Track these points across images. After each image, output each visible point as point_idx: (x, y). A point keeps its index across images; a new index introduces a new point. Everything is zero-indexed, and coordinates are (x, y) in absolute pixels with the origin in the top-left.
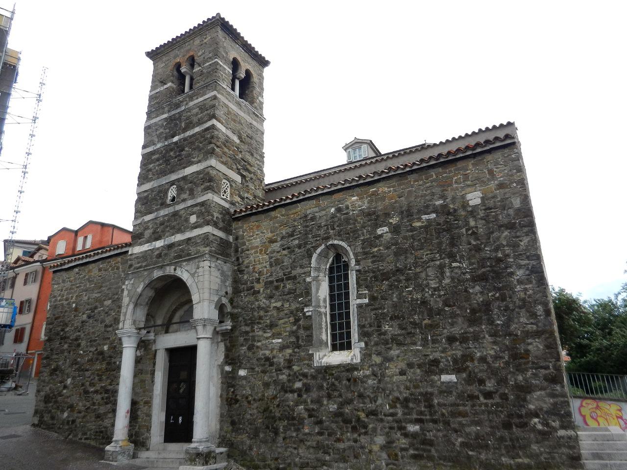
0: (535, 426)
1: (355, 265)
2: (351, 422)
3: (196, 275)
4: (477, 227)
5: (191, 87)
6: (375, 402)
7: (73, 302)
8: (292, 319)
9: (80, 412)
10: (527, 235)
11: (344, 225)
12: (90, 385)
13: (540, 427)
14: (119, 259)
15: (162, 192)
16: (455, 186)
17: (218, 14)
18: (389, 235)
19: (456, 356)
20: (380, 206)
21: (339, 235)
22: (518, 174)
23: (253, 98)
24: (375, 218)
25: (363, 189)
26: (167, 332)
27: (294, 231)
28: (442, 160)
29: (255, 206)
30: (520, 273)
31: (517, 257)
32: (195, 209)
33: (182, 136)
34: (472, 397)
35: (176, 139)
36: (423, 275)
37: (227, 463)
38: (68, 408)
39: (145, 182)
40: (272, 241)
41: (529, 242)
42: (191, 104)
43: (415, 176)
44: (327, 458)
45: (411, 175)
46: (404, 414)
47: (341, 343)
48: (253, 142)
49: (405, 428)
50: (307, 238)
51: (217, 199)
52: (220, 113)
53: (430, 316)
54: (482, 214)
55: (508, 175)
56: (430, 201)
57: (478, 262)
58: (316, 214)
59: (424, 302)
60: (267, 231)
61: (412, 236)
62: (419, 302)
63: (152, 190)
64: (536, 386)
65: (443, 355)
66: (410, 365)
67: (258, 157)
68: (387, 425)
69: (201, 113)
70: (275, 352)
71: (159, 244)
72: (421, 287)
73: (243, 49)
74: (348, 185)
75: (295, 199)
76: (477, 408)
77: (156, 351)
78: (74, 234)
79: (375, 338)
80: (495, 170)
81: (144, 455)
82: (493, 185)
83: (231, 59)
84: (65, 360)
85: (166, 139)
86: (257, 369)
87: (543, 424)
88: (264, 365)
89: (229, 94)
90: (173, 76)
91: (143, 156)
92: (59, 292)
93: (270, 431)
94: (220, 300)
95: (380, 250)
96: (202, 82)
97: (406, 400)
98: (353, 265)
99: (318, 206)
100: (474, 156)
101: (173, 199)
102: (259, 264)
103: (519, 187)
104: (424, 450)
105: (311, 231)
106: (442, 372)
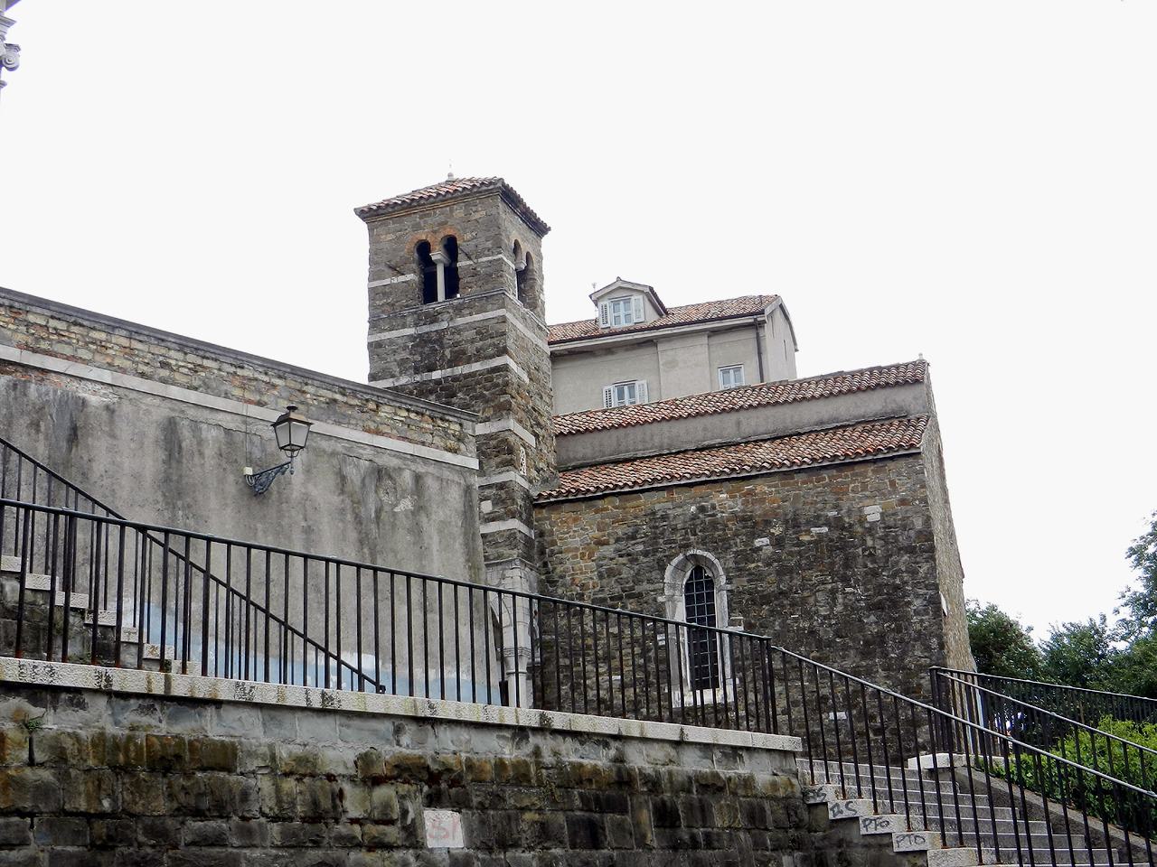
35: (436, 375)
40: (600, 543)
42: (460, 321)
50: (657, 543)
56: (822, 510)
82: (894, 499)
85: (417, 371)
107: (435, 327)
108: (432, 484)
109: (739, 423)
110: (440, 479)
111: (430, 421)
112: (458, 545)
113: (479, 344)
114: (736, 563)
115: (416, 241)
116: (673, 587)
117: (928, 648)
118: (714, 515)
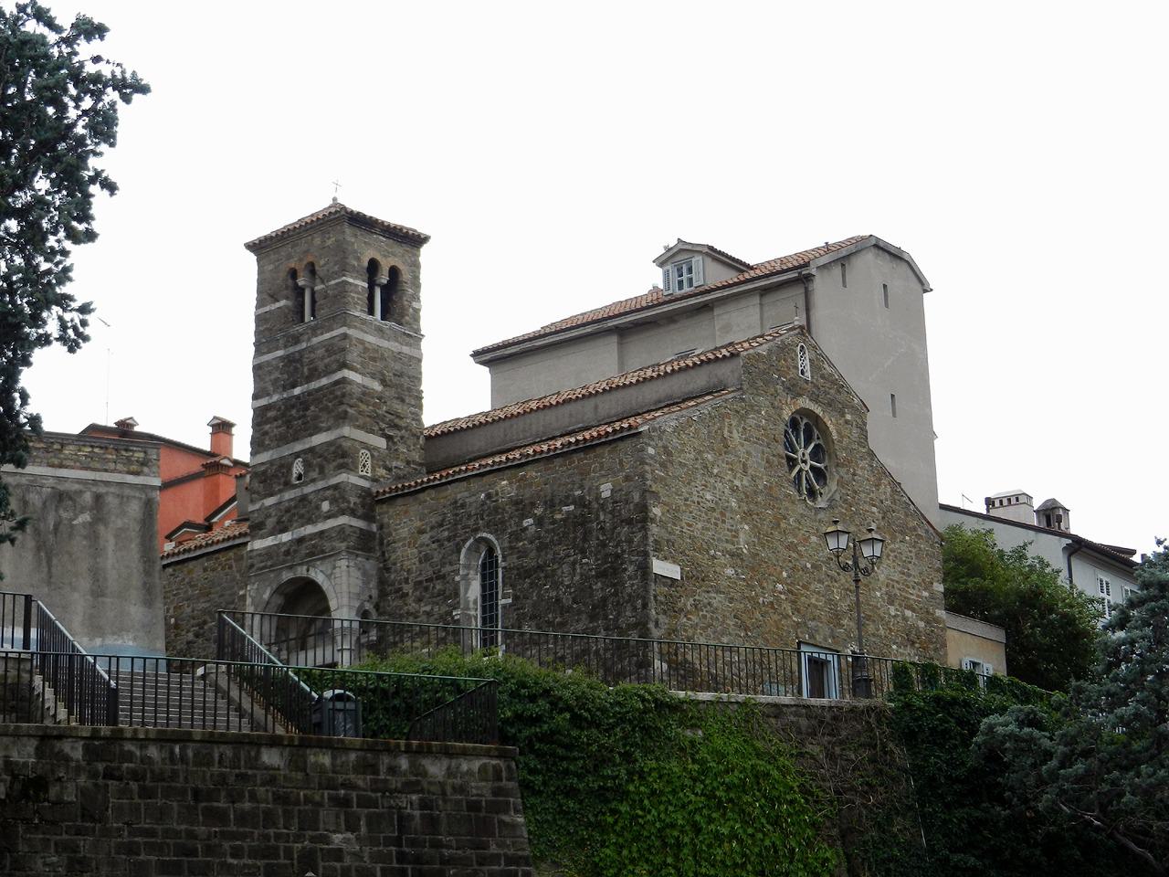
14: (231, 554)
15: (284, 466)
20: (527, 493)
27: (443, 520)
32: (328, 493)
35: (297, 391)
40: (421, 532)
42: (315, 340)
50: (456, 529)
51: (353, 479)
52: (353, 356)
56: (572, 490)
63: (271, 462)
71: (286, 537)
82: (621, 476)
85: (285, 388)
89: (364, 322)
99: (468, 489)
101: (299, 477)
107: (298, 348)
108: (112, 501)
109: (596, 407)
110: (121, 497)
111: (114, 452)
112: (134, 546)
113: (326, 361)
114: (510, 542)
115: (287, 269)
116: (467, 567)
117: (635, 609)
118: (497, 501)
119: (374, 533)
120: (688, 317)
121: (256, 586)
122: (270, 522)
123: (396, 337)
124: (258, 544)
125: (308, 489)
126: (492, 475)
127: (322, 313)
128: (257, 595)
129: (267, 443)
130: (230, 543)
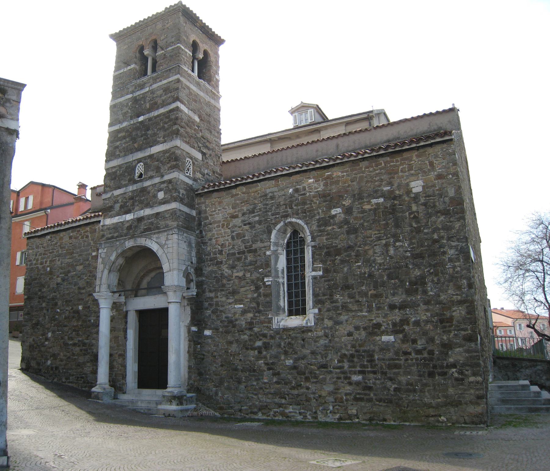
0: (452, 375)
1: (311, 241)
2: (304, 374)
3: (166, 247)
4: (418, 212)
5: (154, 70)
6: (326, 357)
7: (48, 266)
8: (253, 288)
9: (61, 360)
10: (459, 221)
11: (300, 205)
12: (69, 338)
13: (456, 375)
14: (88, 228)
15: (130, 168)
16: (400, 174)
17: (180, 3)
18: (343, 216)
19: (395, 320)
20: (334, 189)
21: (296, 214)
22: (454, 167)
23: (211, 76)
24: (329, 199)
25: (319, 172)
26: (136, 296)
27: (255, 208)
28: (390, 150)
29: (217, 184)
30: (452, 252)
31: (449, 239)
32: (163, 186)
33: (147, 116)
34: (406, 353)
35: (141, 119)
36: (371, 252)
37: (195, 405)
38: (51, 357)
39: (112, 158)
40: (234, 217)
41: (460, 226)
42: (155, 86)
43: (366, 163)
44: (283, 401)
45: (363, 162)
46: (350, 367)
47: (297, 308)
48: (212, 120)
49: (350, 378)
50: (267, 215)
51: (182, 177)
52: (183, 95)
53: (376, 287)
54: (422, 200)
55: (445, 167)
56: (379, 186)
57: (418, 242)
58: (275, 194)
59: (371, 276)
60: (229, 208)
61: (363, 217)
62: (366, 275)
63: (120, 166)
64: (456, 344)
65: (385, 320)
66: (357, 328)
67: (216, 134)
68: (336, 376)
69: (165, 95)
70: (237, 316)
71: (129, 217)
72: (369, 262)
73: (201, 31)
74: (305, 168)
75: (255, 179)
76: (410, 361)
77: (127, 312)
78: (15, 195)
79: (328, 305)
80: (435, 162)
81: (124, 397)
82: (432, 175)
83: (191, 42)
84: (45, 317)
85: (132, 118)
86: (221, 330)
87: (459, 373)
88: (227, 327)
89: (190, 76)
90: (136, 57)
91: (110, 133)
92: (34, 257)
93: (233, 381)
94: (187, 268)
95: (333, 229)
96: (164, 65)
97: (352, 356)
98: (309, 242)
99: (277, 186)
100: (418, 148)
101: (141, 175)
102: (222, 237)
103: (454, 178)
104: (365, 394)
105: (270, 209)
106: (383, 333)
109: (337, 146)
113: (163, 98)
118: (304, 194)
119: (194, 217)
120: (306, 136)
121: (105, 251)
122: (117, 207)
123: (207, 92)
124: (108, 222)
125: (147, 184)
126: (298, 175)
127: (160, 69)
128: (106, 258)
129: (117, 153)
130: (88, 221)
